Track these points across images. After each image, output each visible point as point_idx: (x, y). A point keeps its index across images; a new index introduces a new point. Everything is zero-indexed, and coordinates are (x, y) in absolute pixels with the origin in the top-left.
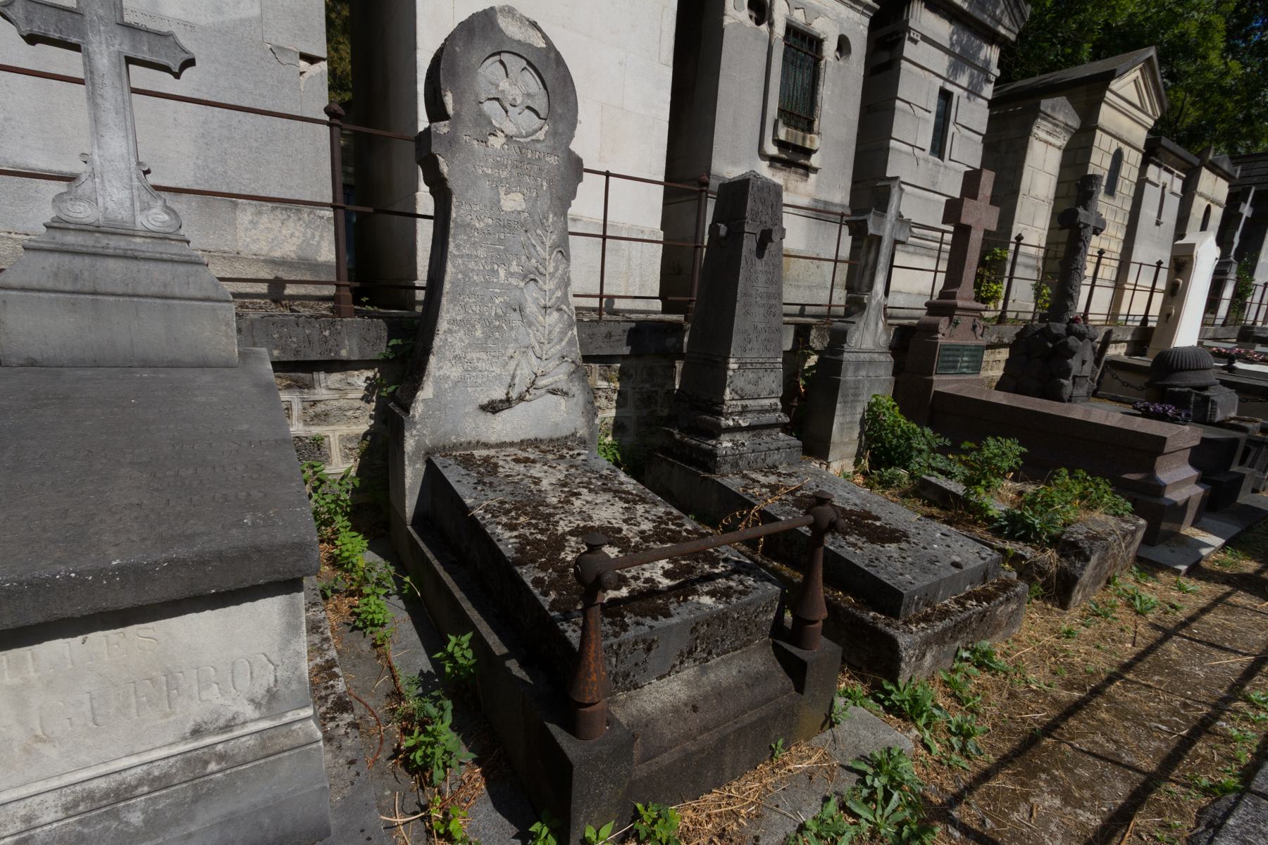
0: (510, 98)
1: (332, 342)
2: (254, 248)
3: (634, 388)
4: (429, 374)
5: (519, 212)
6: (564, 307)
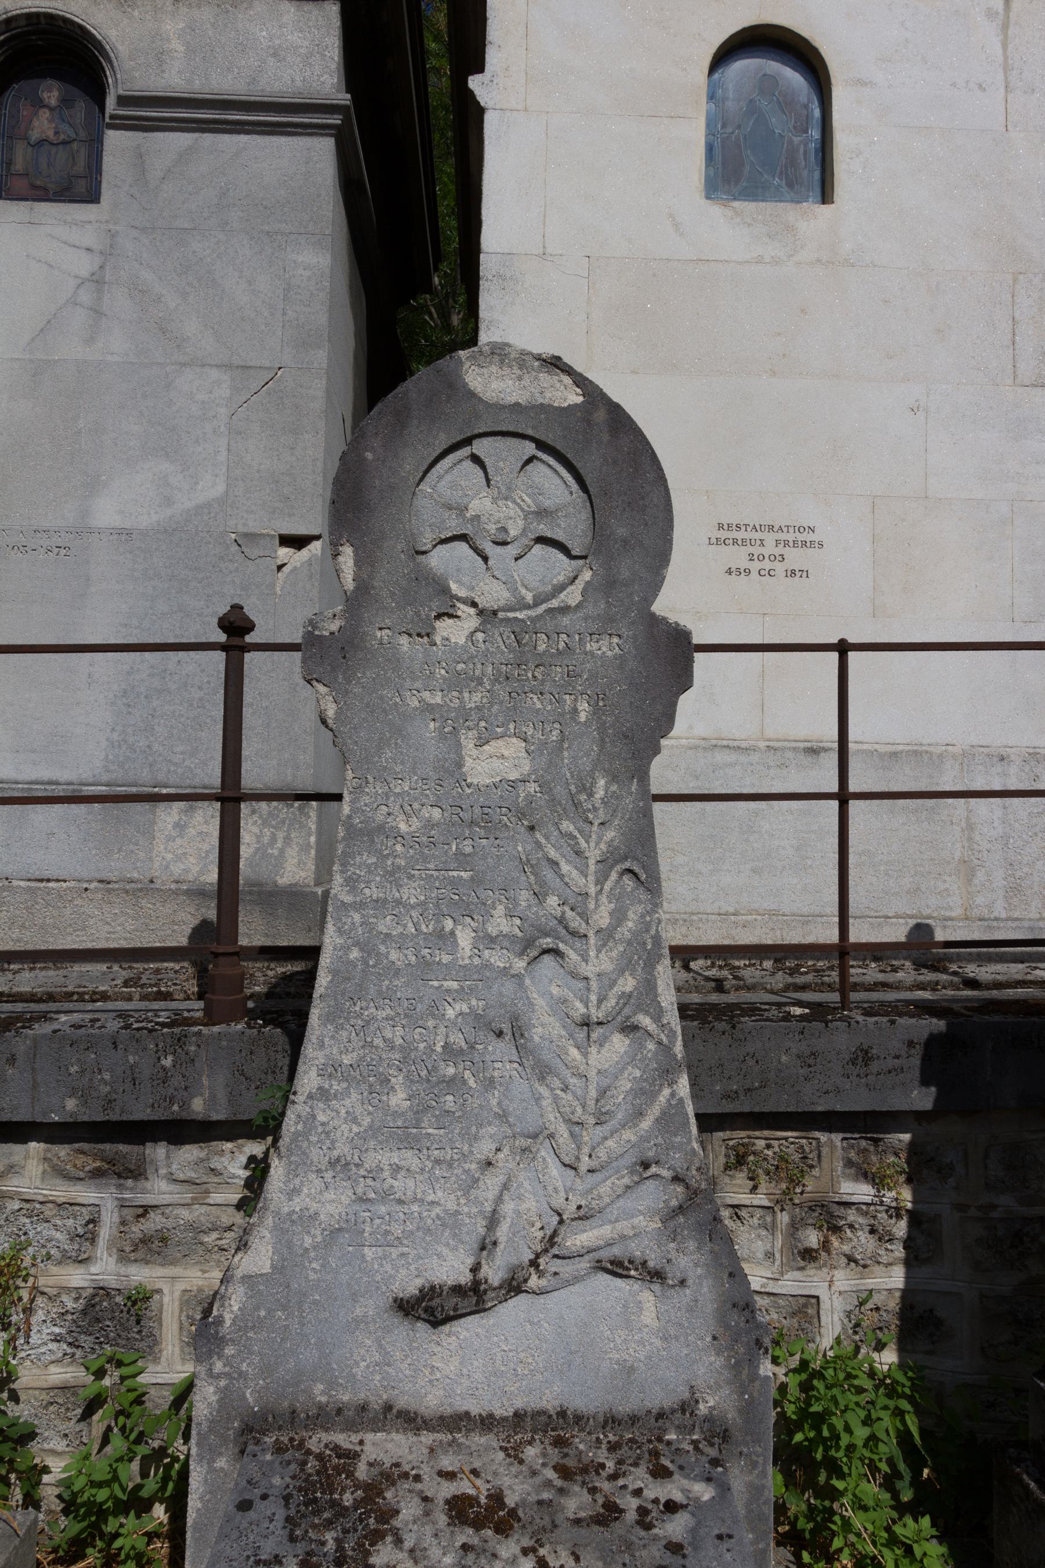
0: (492, 528)
1: (176, 1081)
2: (177, 869)
3: (961, 1208)
4: (265, 1208)
5: (513, 784)
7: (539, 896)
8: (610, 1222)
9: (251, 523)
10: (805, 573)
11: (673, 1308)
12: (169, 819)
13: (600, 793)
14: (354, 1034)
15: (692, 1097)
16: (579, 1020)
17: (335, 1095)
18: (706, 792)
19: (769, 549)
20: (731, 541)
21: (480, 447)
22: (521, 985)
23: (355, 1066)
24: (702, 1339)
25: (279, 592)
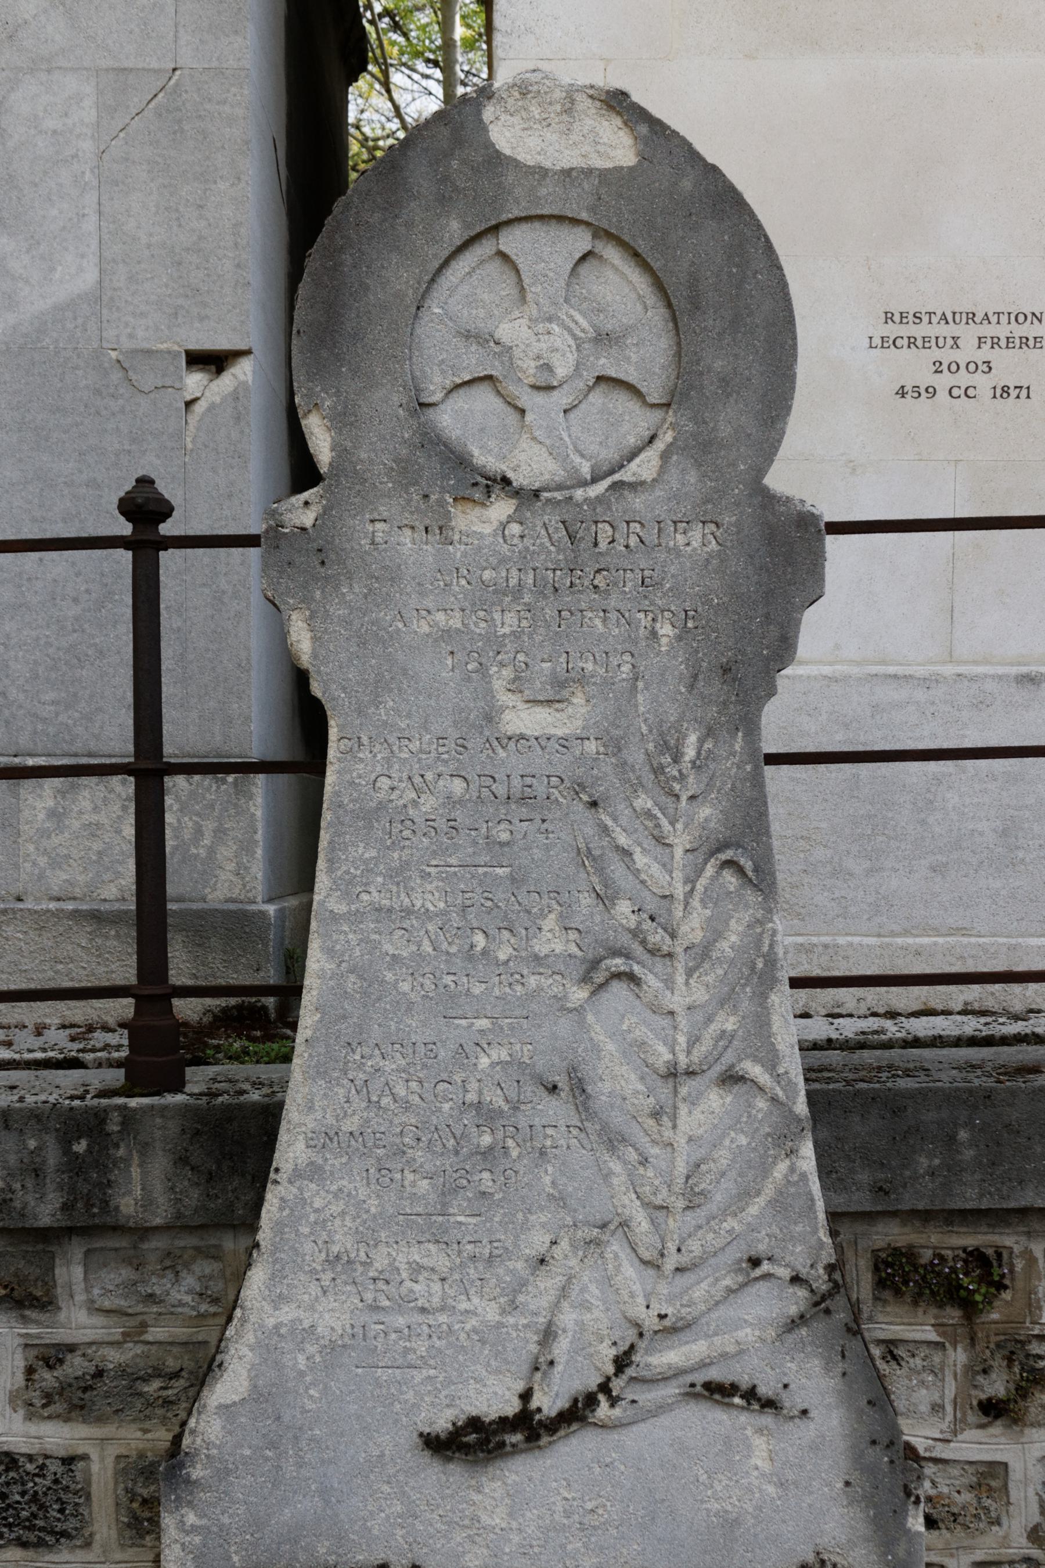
2: (57, 879)
6: (755, 1071)
7: (605, 899)
8: (707, 1336)
9: (140, 333)
10: (1024, 391)
11: (791, 1446)
12: (39, 805)
13: (690, 753)
14: (353, 1091)
15: (820, 1172)
16: (663, 1070)
17: (332, 1173)
18: (861, 748)
19: (968, 352)
20: (905, 342)
21: (511, 241)
22: (582, 1022)
23: (357, 1134)
24: (829, 1485)
25: (190, 446)
